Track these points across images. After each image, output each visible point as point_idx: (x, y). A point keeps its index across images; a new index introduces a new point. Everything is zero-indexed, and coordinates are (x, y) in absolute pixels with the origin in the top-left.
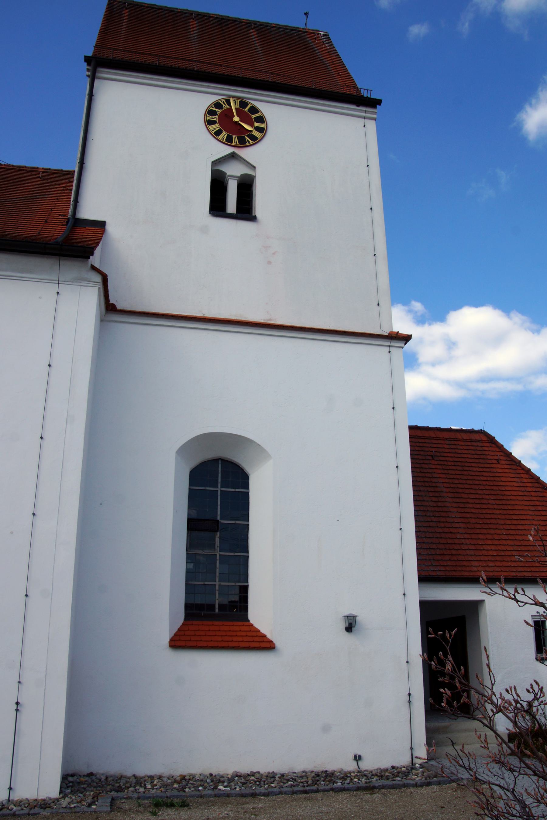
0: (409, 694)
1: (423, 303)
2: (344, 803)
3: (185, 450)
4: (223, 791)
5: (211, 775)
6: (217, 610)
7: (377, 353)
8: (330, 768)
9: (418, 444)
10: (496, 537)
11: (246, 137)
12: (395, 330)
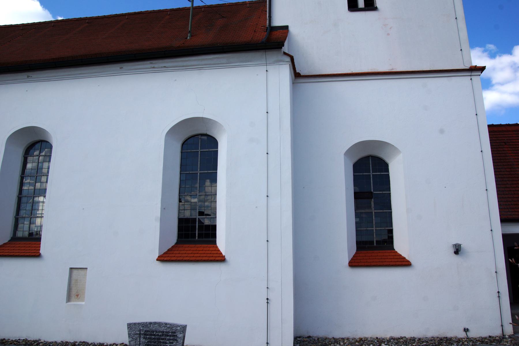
0: (499, 292)
1: (495, 45)
3: (349, 153)
5: (377, 338)
6: (375, 244)
7: (463, 81)
8: (449, 335)
9: (494, 136)
12: (474, 64)
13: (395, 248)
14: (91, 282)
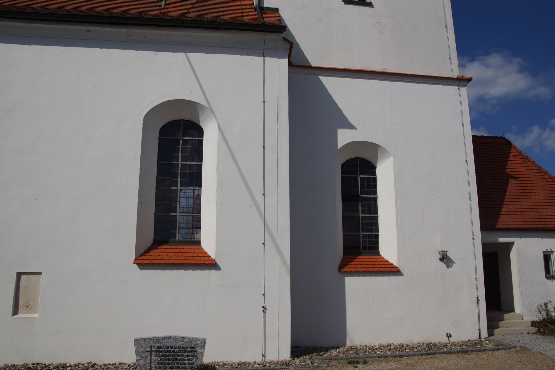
2: (453, 360)
10: (519, 203)
13: (381, 253)
14: (43, 289)
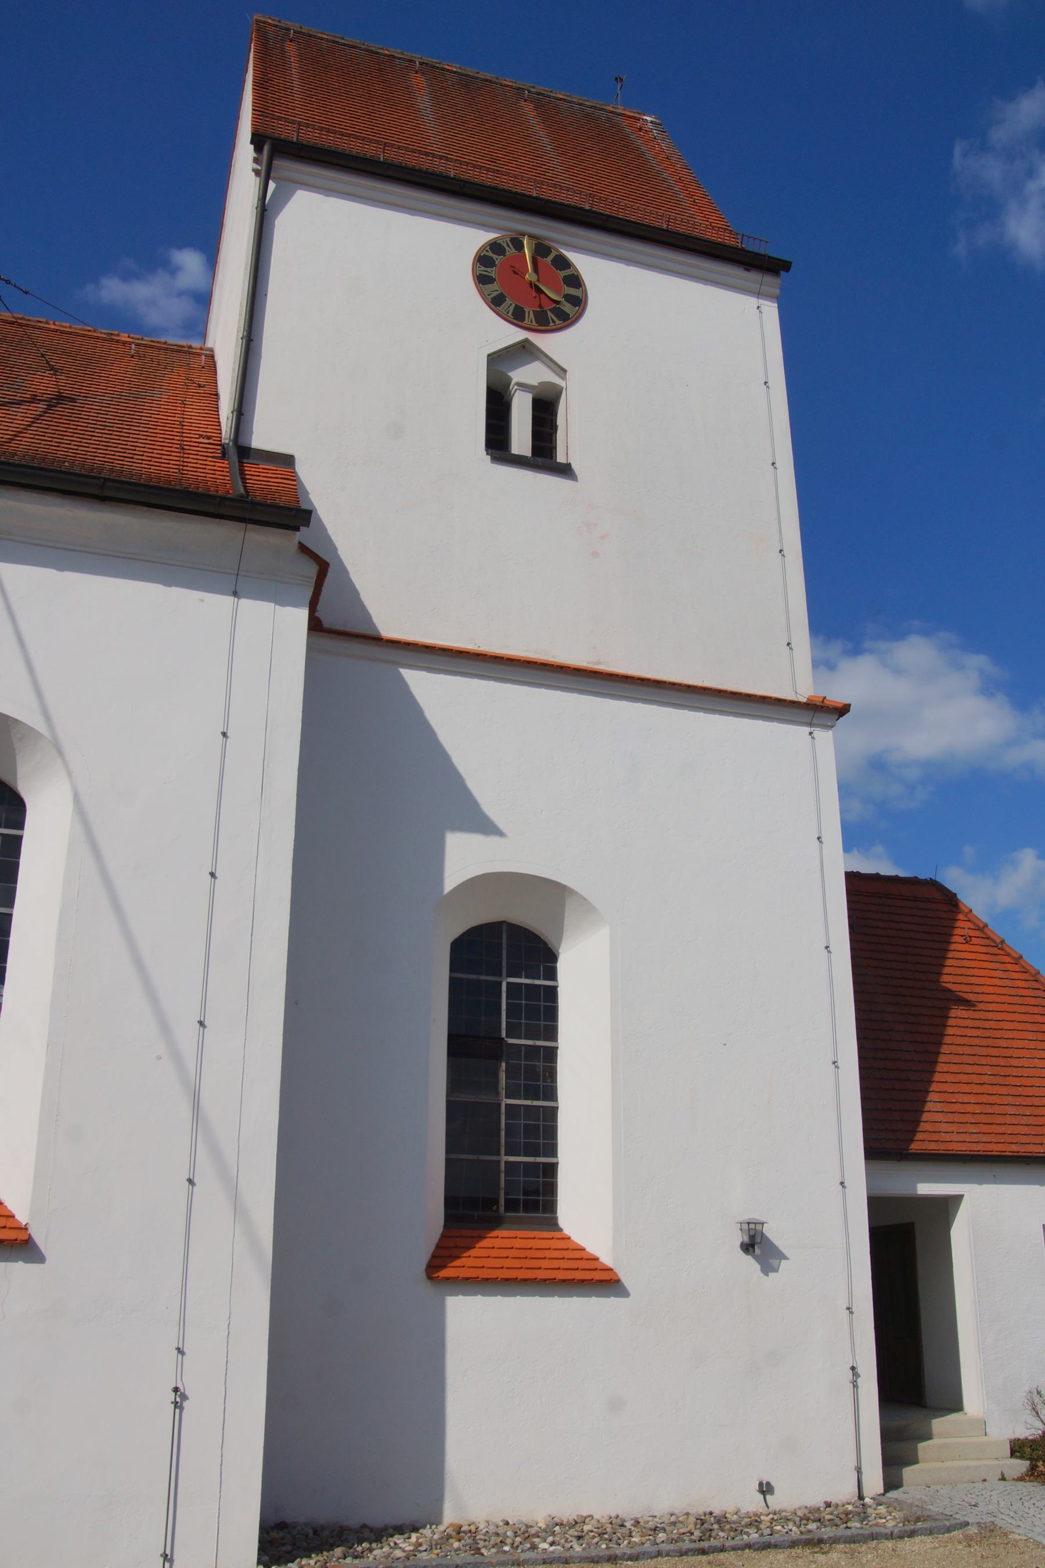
4: (553, 1552)
11: (550, 314)
